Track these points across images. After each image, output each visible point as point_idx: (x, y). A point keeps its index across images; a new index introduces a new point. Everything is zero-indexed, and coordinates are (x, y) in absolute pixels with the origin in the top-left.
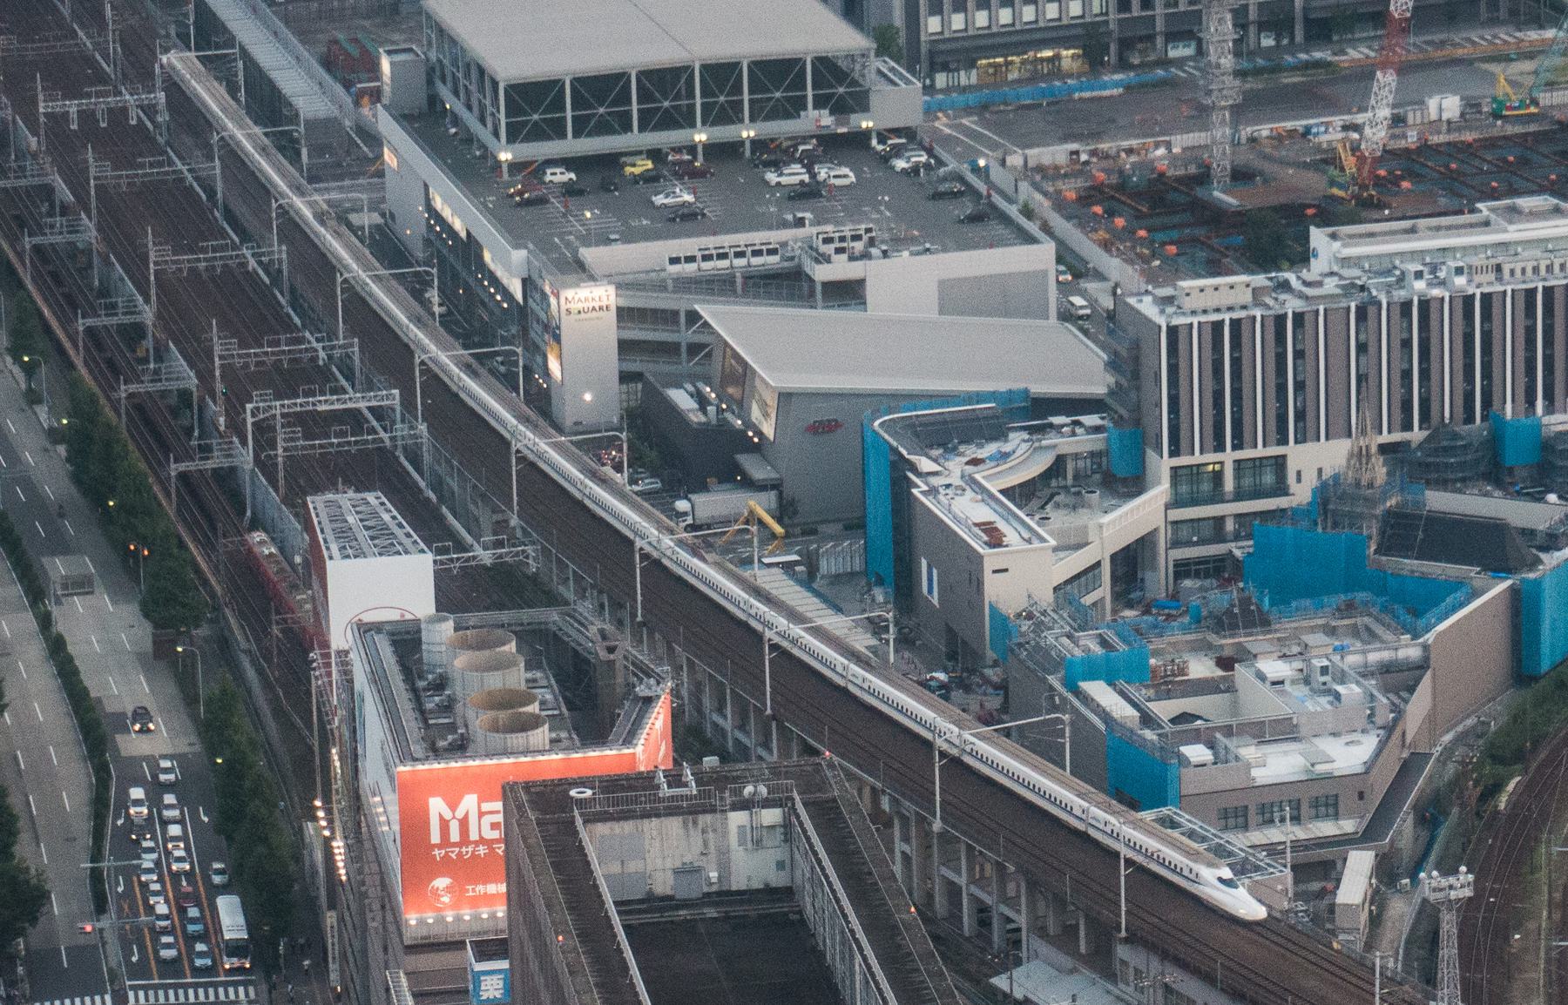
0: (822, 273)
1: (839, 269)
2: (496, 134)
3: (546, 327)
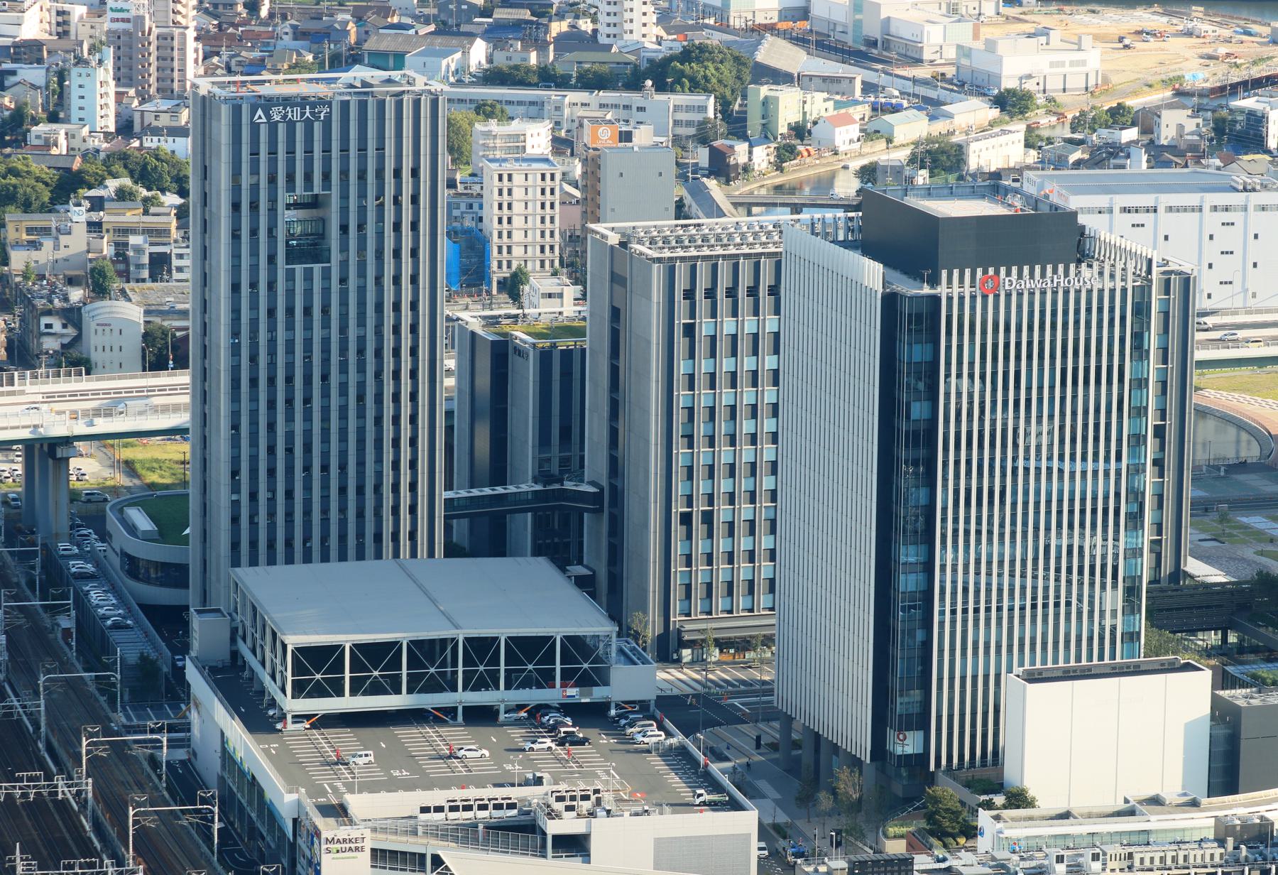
0: (553, 828)
1: (567, 825)
2: (283, 690)
3: (310, 863)
